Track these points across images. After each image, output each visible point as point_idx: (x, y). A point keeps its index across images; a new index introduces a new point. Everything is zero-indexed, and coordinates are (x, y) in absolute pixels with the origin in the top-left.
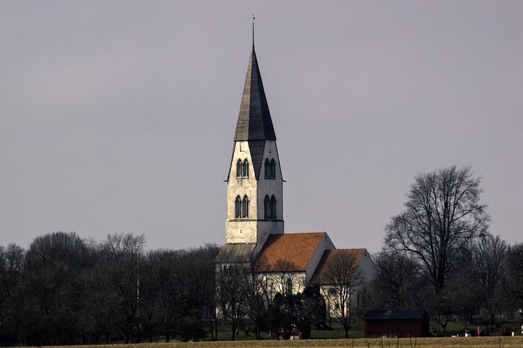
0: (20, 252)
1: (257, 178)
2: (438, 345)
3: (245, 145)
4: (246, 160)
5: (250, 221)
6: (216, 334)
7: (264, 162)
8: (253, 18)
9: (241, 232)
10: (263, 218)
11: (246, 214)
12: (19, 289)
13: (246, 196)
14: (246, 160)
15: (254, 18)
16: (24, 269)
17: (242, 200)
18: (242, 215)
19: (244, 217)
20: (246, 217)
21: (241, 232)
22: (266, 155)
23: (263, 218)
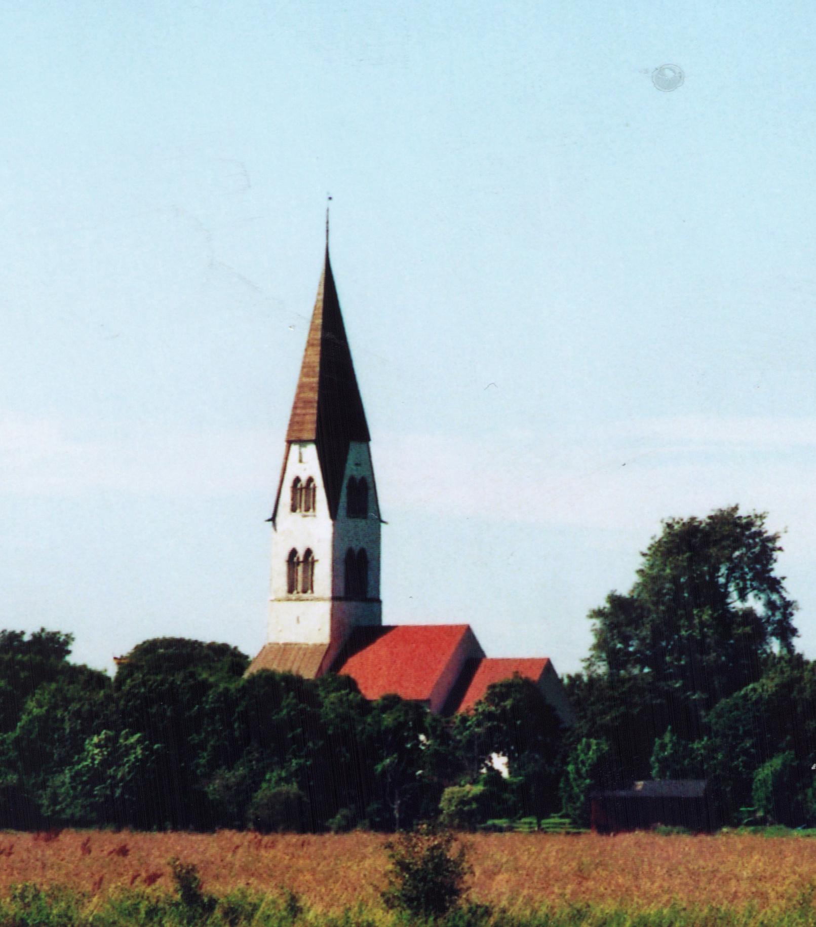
0: (221, 880)
1: (333, 514)
2: (404, 838)
3: (311, 452)
4: (310, 480)
5: (318, 599)
6: (525, 823)
7: (345, 482)
8: (326, 199)
9: (301, 461)
10: (342, 594)
11: (308, 587)
12: (59, 917)
13: (309, 552)
14: (310, 480)
15: (330, 198)
16: (589, 862)
17: (301, 559)
18: (300, 588)
19: (305, 591)
20: (309, 591)
21: (301, 461)
22: (351, 470)
23: (342, 594)
